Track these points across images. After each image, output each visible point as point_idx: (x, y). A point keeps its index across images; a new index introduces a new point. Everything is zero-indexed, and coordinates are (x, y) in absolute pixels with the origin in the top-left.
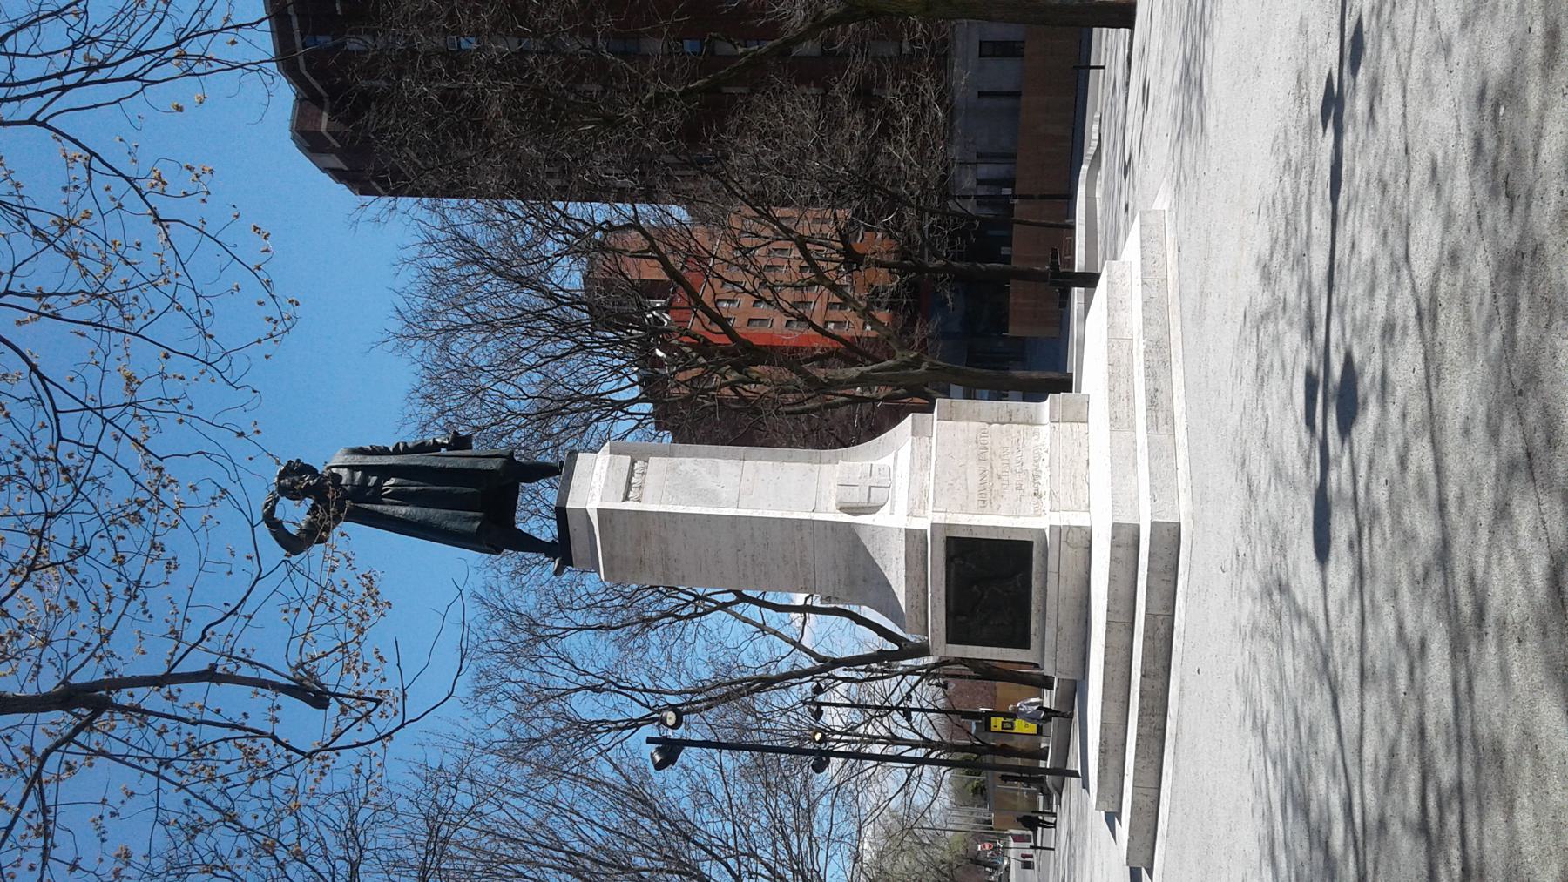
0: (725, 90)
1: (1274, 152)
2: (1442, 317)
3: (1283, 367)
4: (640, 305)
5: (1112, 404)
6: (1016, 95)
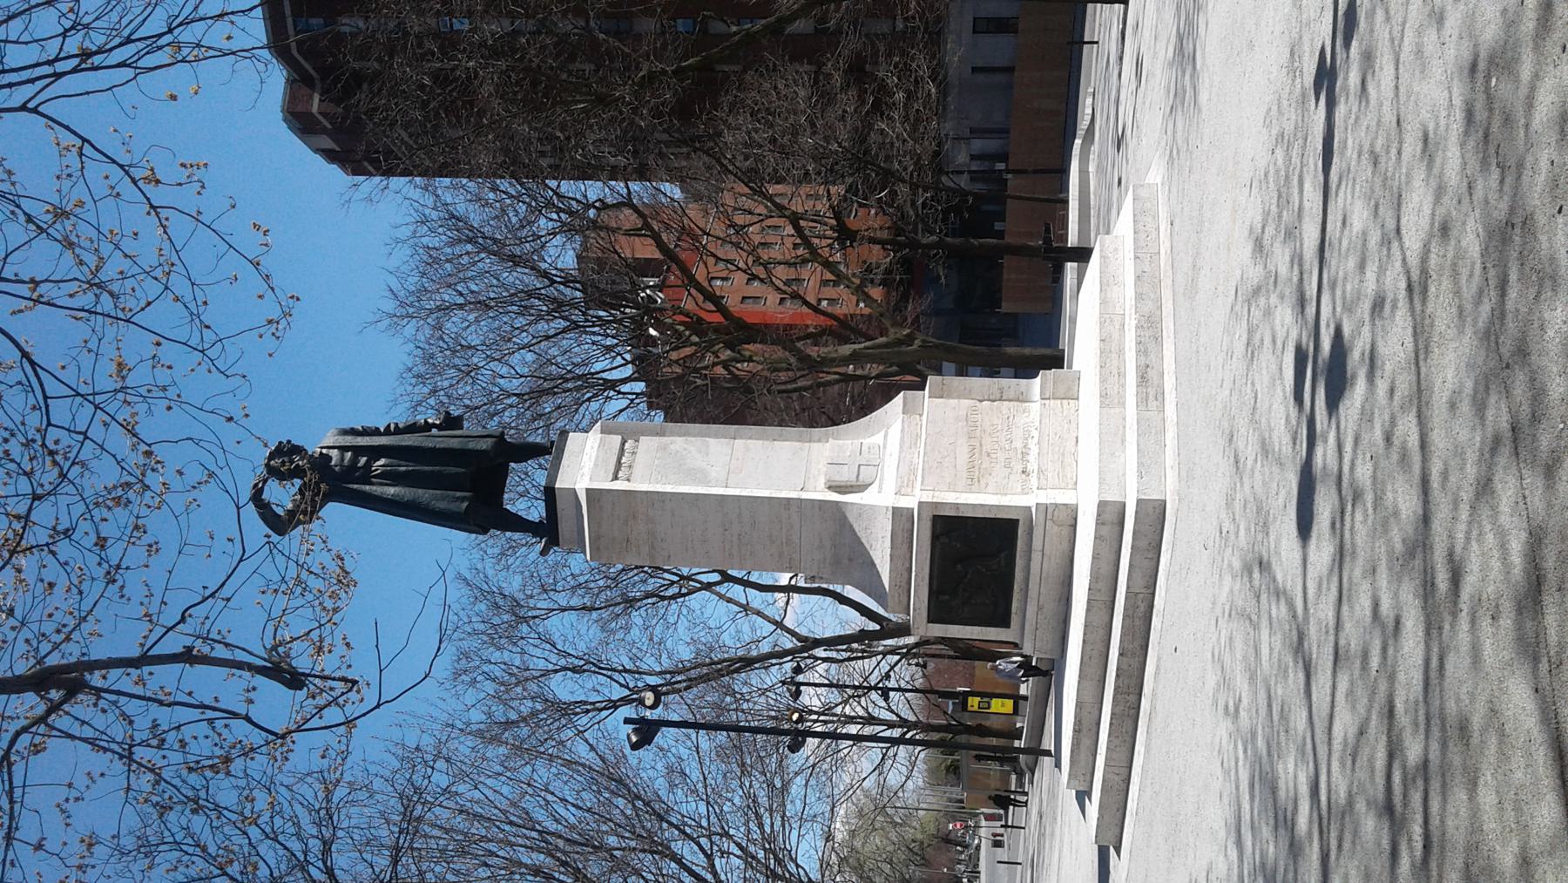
0: (718, 67)
1: (1267, 124)
2: (1432, 289)
3: (1274, 342)
4: (633, 283)
5: (1103, 381)
6: (1009, 70)
